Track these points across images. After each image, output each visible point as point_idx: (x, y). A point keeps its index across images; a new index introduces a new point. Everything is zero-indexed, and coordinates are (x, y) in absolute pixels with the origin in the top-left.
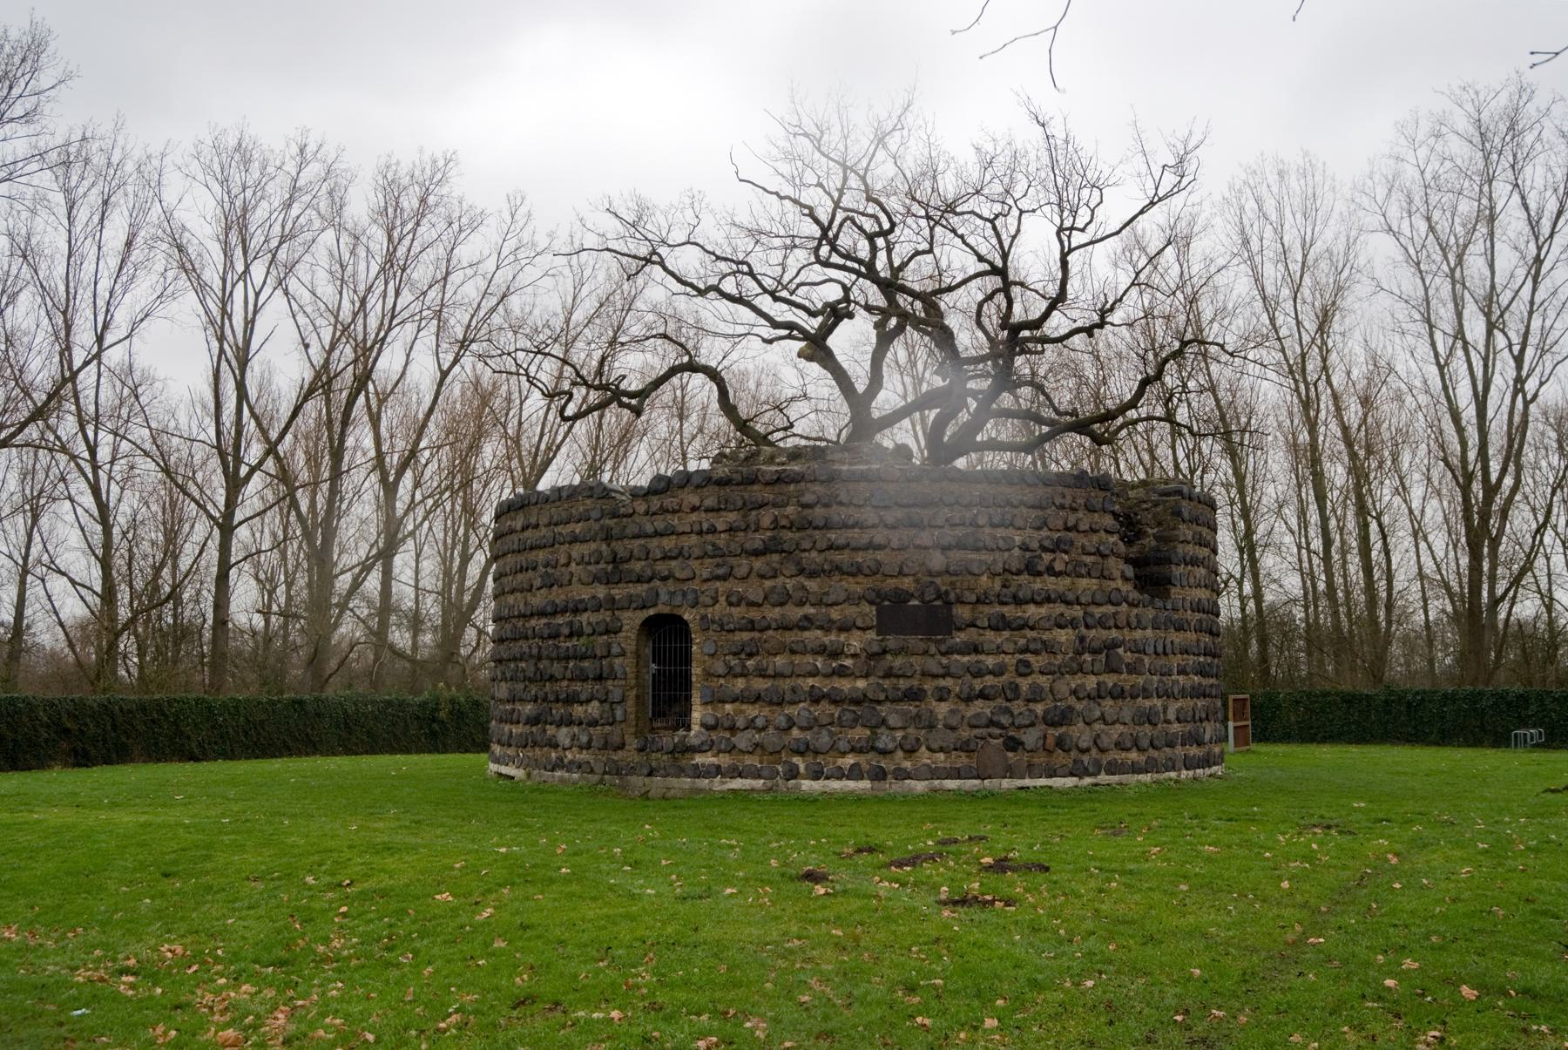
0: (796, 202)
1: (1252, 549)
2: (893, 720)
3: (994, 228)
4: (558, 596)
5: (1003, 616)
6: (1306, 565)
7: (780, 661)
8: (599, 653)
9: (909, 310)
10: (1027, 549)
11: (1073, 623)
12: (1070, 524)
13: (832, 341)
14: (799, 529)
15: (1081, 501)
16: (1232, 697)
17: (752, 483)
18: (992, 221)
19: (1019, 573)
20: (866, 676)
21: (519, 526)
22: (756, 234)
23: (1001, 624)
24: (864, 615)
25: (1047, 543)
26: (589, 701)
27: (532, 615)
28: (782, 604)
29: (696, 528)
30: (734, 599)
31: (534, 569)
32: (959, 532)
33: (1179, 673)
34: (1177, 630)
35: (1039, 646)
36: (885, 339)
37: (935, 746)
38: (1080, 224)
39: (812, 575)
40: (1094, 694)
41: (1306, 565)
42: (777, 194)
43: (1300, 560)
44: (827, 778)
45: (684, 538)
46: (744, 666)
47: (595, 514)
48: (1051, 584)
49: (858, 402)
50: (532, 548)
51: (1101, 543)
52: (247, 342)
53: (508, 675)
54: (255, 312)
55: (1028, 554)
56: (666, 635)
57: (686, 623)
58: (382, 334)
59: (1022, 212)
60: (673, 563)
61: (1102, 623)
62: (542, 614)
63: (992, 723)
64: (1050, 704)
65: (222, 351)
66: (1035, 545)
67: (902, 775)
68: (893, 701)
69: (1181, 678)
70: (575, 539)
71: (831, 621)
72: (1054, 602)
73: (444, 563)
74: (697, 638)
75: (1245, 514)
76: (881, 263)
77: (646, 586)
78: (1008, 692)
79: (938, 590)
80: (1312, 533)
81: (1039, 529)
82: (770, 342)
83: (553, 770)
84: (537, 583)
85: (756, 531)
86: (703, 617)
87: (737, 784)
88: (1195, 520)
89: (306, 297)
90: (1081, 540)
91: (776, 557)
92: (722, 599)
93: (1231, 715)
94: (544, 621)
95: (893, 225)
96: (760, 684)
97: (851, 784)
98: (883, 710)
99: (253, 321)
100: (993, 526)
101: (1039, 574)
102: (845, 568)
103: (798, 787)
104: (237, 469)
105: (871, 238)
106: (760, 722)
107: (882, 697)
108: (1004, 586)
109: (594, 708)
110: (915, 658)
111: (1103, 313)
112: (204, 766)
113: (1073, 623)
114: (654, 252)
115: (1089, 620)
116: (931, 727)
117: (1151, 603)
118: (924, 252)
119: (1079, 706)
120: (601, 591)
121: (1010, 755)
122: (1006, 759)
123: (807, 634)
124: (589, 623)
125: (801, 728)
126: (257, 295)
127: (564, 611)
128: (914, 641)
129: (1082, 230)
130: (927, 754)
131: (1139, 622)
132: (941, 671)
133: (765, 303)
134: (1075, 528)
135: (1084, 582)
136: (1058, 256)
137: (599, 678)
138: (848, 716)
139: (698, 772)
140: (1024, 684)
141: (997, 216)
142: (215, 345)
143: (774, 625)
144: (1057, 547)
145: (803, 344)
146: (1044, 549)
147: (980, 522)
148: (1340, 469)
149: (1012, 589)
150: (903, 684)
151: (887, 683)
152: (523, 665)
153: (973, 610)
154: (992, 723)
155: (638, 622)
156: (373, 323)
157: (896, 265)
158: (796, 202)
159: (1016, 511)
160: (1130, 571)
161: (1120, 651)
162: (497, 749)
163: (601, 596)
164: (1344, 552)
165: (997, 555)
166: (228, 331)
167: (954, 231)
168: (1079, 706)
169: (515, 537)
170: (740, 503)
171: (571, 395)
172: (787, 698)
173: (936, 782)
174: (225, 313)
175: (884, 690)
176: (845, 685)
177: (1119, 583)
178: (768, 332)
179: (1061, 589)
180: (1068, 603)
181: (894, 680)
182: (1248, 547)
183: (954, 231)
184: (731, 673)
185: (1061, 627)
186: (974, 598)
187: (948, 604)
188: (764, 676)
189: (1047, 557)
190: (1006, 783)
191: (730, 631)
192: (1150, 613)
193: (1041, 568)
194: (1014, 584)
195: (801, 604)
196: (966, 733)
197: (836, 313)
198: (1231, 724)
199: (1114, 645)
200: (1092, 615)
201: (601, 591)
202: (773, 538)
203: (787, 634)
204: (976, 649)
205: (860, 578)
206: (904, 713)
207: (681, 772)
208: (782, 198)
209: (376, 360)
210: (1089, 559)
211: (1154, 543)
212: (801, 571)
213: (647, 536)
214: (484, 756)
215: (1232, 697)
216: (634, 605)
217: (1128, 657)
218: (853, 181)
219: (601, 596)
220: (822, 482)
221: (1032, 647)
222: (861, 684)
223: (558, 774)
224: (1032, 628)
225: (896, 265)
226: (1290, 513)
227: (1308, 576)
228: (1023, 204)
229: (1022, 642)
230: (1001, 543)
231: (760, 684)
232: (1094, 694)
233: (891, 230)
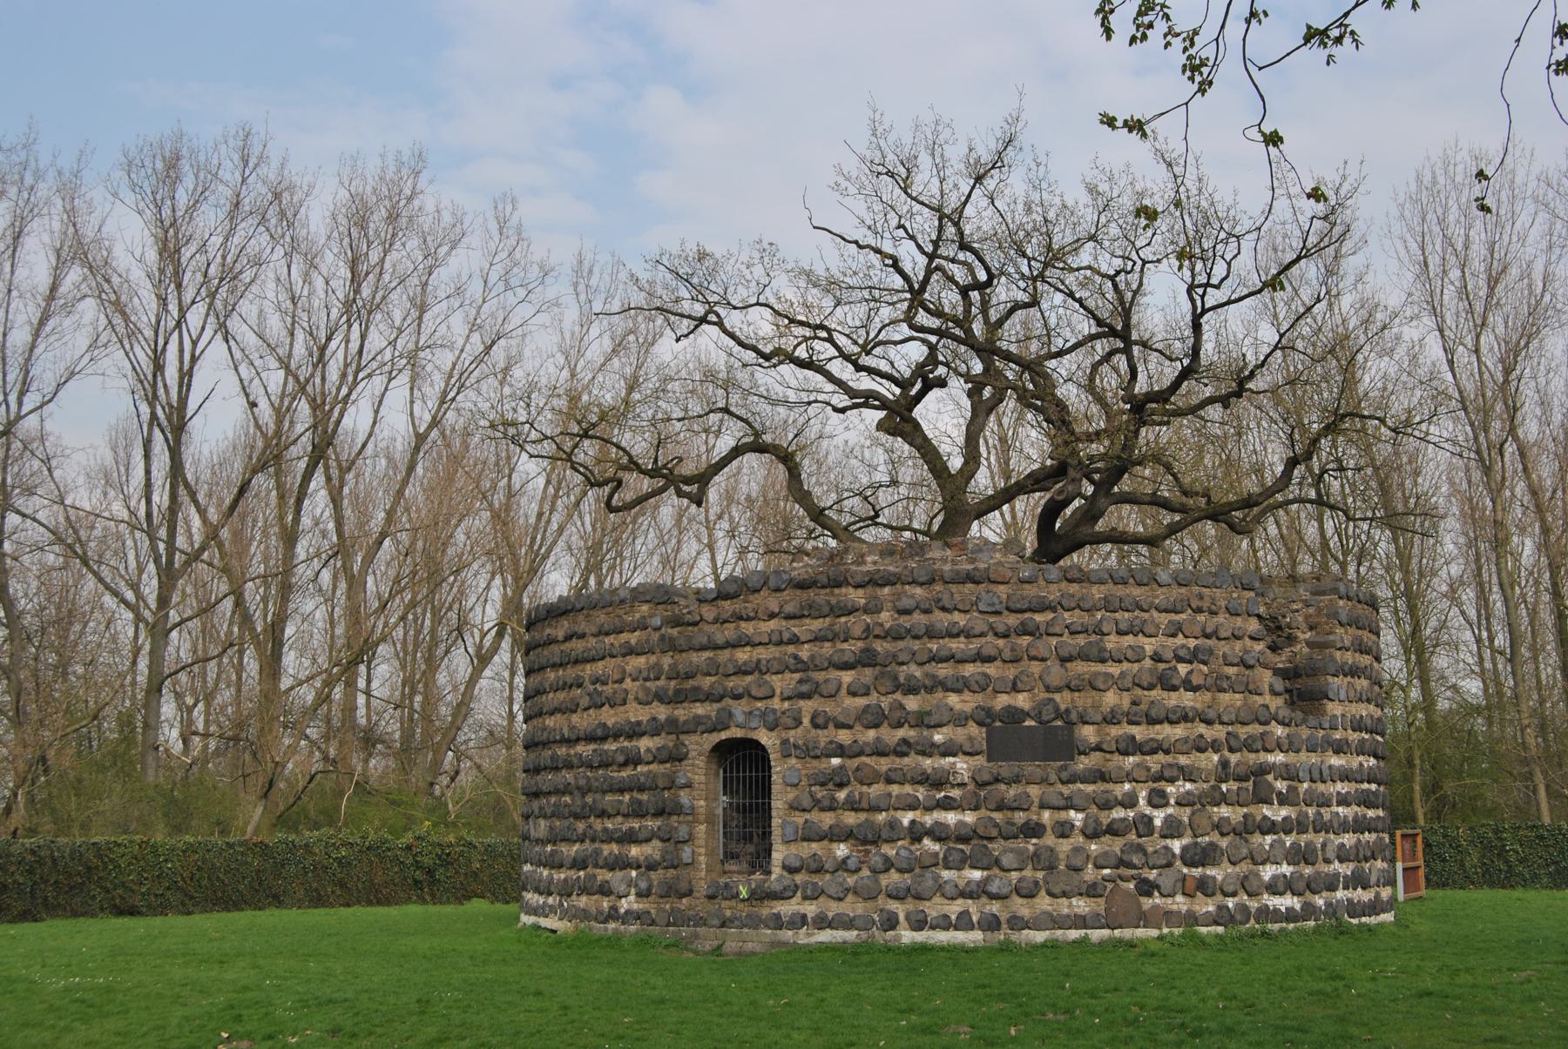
0: (878, 251)
1: (1420, 652)
2: (1006, 860)
3: (1115, 286)
4: (610, 717)
5: (1134, 738)
6: (1488, 665)
7: (876, 790)
8: (661, 784)
9: (1009, 378)
10: (1160, 660)
11: (1215, 746)
12: (1208, 630)
13: (918, 412)
14: (895, 639)
15: (1223, 604)
16: (1398, 833)
17: (839, 586)
18: (1112, 278)
19: (1151, 687)
20: (976, 808)
21: (561, 634)
22: (831, 285)
23: (1130, 747)
24: (971, 739)
25: (1182, 653)
26: (648, 840)
27: (578, 740)
28: (876, 726)
29: (775, 638)
30: (820, 720)
31: (580, 686)
32: (1081, 640)
33: (1339, 804)
34: (1337, 752)
35: (1175, 773)
36: (981, 411)
37: (1057, 890)
38: (1214, 281)
39: (911, 690)
40: (1240, 828)
41: (1488, 665)
42: (856, 242)
43: (1481, 659)
44: (933, 928)
45: (760, 649)
46: (833, 799)
47: (657, 621)
48: (1187, 699)
49: (951, 485)
50: (576, 662)
51: (1246, 652)
52: (183, 401)
53: (549, 811)
54: (194, 359)
55: (1162, 666)
56: (743, 764)
57: (763, 748)
58: (344, 391)
59: (1144, 262)
60: (749, 679)
61: (1249, 746)
62: (590, 738)
63: (1121, 863)
64: (1186, 841)
65: (154, 416)
66: (1169, 655)
67: (1017, 923)
68: (1006, 839)
69: (1340, 809)
70: (630, 651)
71: (933, 745)
72: (1192, 721)
73: (403, 667)
74: (778, 769)
75: (1412, 609)
76: (978, 328)
77: (716, 706)
78: (1141, 827)
79: (1057, 709)
80: (1497, 627)
81: (1174, 635)
82: (843, 411)
83: (605, 921)
84: (585, 702)
85: (846, 640)
86: (785, 742)
87: (826, 936)
88: (1354, 622)
89: (251, 340)
90: (1223, 648)
91: (868, 671)
92: (806, 721)
93: (1399, 854)
94: (592, 747)
95: (991, 276)
96: (851, 819)
97: (960, 937)
98: (996, 848)
99: (190, 373)
100: (1120, 633)
101: (1174, 688)
102: (949, 684)
103: (898, 937)
104: (170, 562)
105: (964, 292)
106: (852, 864)
107: (994, 833)
108: (1134, 703)
109: (652, 850)
110: (1033, 791)
111: (1241, 383)
112: (85, 923)
113: (1215, 746)
114: (710, 311)
115: (1233, 743)
116: (1051, 868)
117: (1304, 721)
118: (1026, 306)
119: (1224, 843)
120: (662, 712)
121: (1144, 900)
122: (1139, 905)
123: (906, 760)
124: (648, 750)
125: (900, 871)
126: (195, 343)
127: (616, 736)
128: (1031, 768)
129: (1217, 287)
130: (1048, 899)
131: (1291, 743)
132: (1062, 803)
133: (840, 369)
134: (1214, 635)
135: (1225, 698)
136: (1189, 318)
137: (659, 813)
138: (955, 857)
139: (778, 922)
140: (1159, 818)
141: (1118, 273)
142: (145, 409)
143: (868, 750)
144: (1194, 657)
145: (881, 414)
146: (1180, 660)
147: (1105, 630)
148: (1528, 543)
149: (1144, 707)
150: (1020, 817)
151: (998, 816)
152: (568, 799)
153: (1098, 732)
154: (1121, 863)
155: (708, 747)
156: (333, 374)
157: (993, 319)
158: (878, 251)
159: (1146, 615)
160: (1279, 685)
161: (1270, 778)
162: (531, 897)
163: (662, 717)
164: (1535, 650)
165: (1126, 665)
166: (161, 392)
167: (1071, 295)
168: (1224, 843)
169: (555, 648)
170: (826, 610)
171: (620, 483)
172: (884, 836)
173: (1059, 932)
174: (159, 367)
175: (996, 825)
176: (951, 818)
177: (1267, 699)
178: (841, 400)
179: (1199, 706)
180: (1209, 722)
181: (1009, 814)
182: (1417, 649)
183: (1071, 295)
184: (817, 805)
185: (1201, 750)
186: (1099, 718)
187: (1070, 724)
188: (856, 810)
189: (1183, 669)
190: (1140, 932)
191: (816, 757)
192: (1305, 732)
193: (1176, 682)
194: (1145, 700)
195: (899, 725)
196: (1090, 873)
197: (926, 379)
198: (1399, 866)
199: (1262, 770)
200: (1236, 737)
201: (662, 712)
202: (866, 650)
203: (883, 760)
204: (1101, 776)
205: (967, 695)
206: (1019, 852)
207: (755, 922)
208: (860, 247)
209: (338, 422)
210: (1231, 671)
211: (1306, 650)
212: (898, 687)
213: (716, 647)
214: (513, 907)
215: (1398, 833)
216: (700, 728)
217: (1281, 786)
218: (950, 230)
219: (662, 717)
220: (921, 584)
221: (1167, 774)
222: (969, 818)
223: (612, 925)
224: (1167, 752)
225: (993, 319)
226: (1468, 594)
227: (1490, 679)
228: (1147, 254)
229: (1155, 768)
230: (1130, 654)
231: (851, 819)
232: (1240, 828)
233: (989, 283)
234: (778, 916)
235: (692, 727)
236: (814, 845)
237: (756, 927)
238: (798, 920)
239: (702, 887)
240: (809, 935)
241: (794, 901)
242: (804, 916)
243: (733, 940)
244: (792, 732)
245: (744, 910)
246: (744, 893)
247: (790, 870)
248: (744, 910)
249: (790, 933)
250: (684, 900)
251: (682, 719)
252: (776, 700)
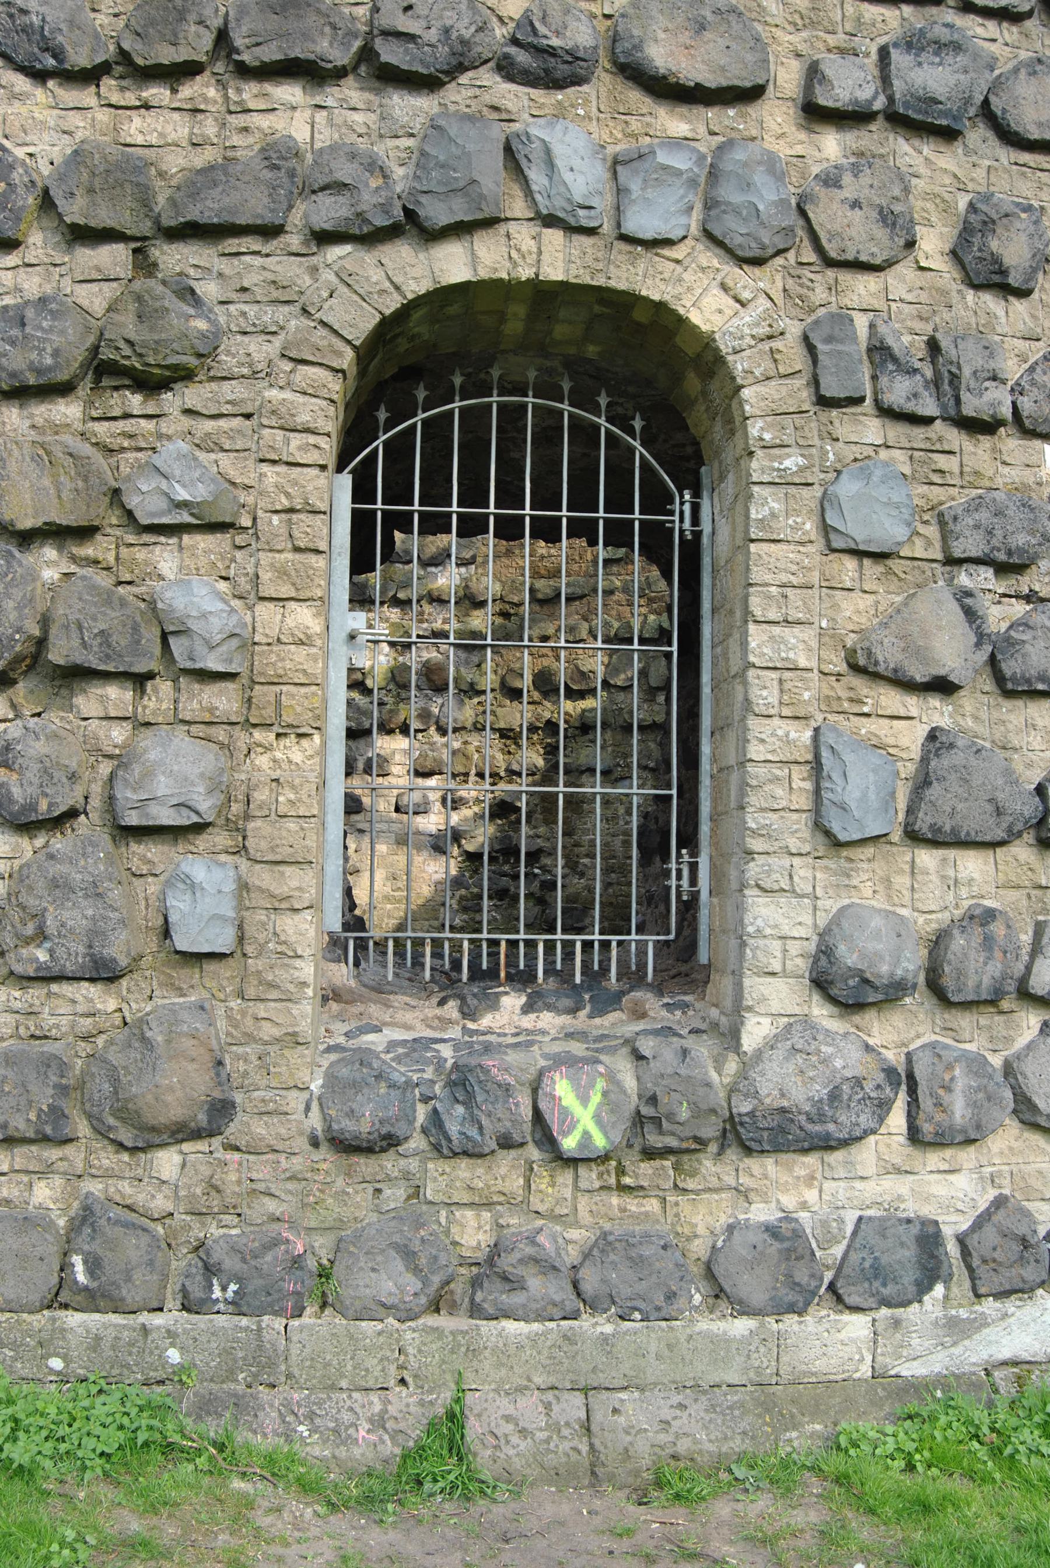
57: (708, 360)
234: (786, 1239)
235: (255, 206)
236: (972, 865)
237: (662, 1310)
238: (904, 1256)
239: (292, 1098)
240: (957, 1329)
241: (865, 1155)
242: (929, 1238)
243: (511, 1380)
244: (863, 288)
245: (573, 1216)
246: (584, 1117)
247: (843, 987)
248: (573, 1216)
249: (857, 1326)
250: (167, 1162)
251: (175, 162)
252: (775, 122)
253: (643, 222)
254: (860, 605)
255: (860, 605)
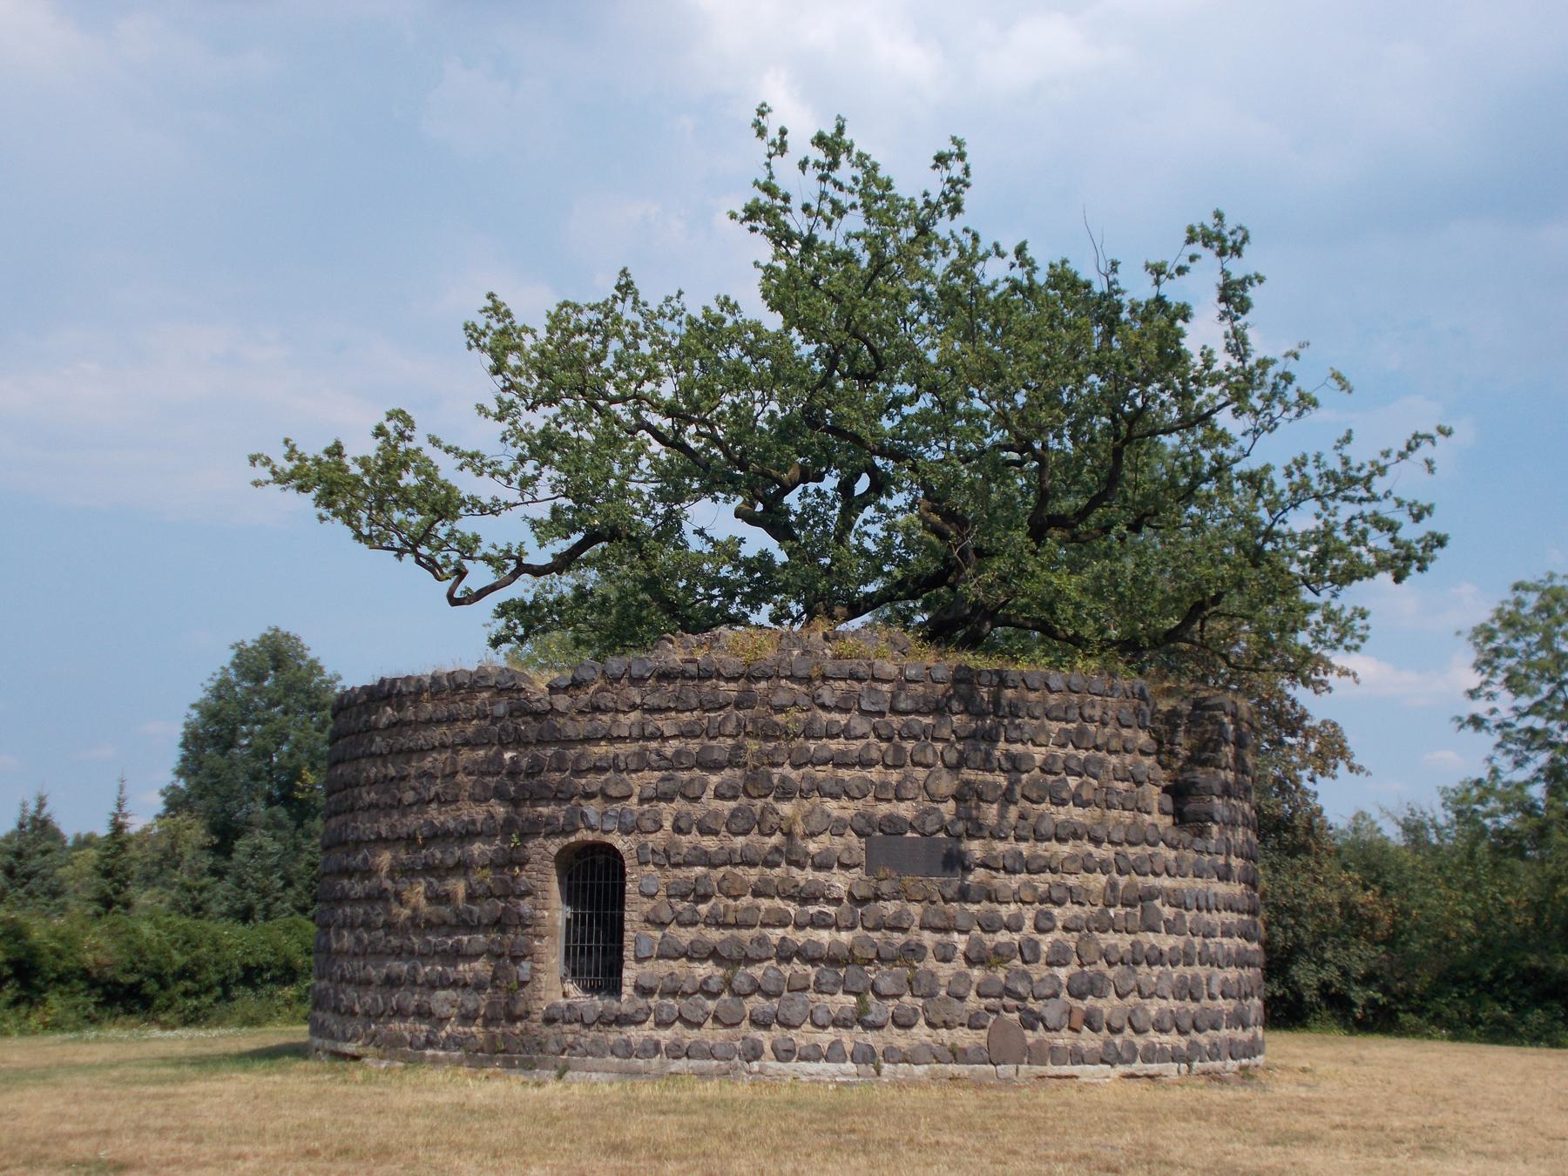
237: (602, 1056)
238: (650, 1047)
242: (657, 1044)
244: (651, 837)
253: (607, 827)
254: (648, 905)
255: (648, 905)
